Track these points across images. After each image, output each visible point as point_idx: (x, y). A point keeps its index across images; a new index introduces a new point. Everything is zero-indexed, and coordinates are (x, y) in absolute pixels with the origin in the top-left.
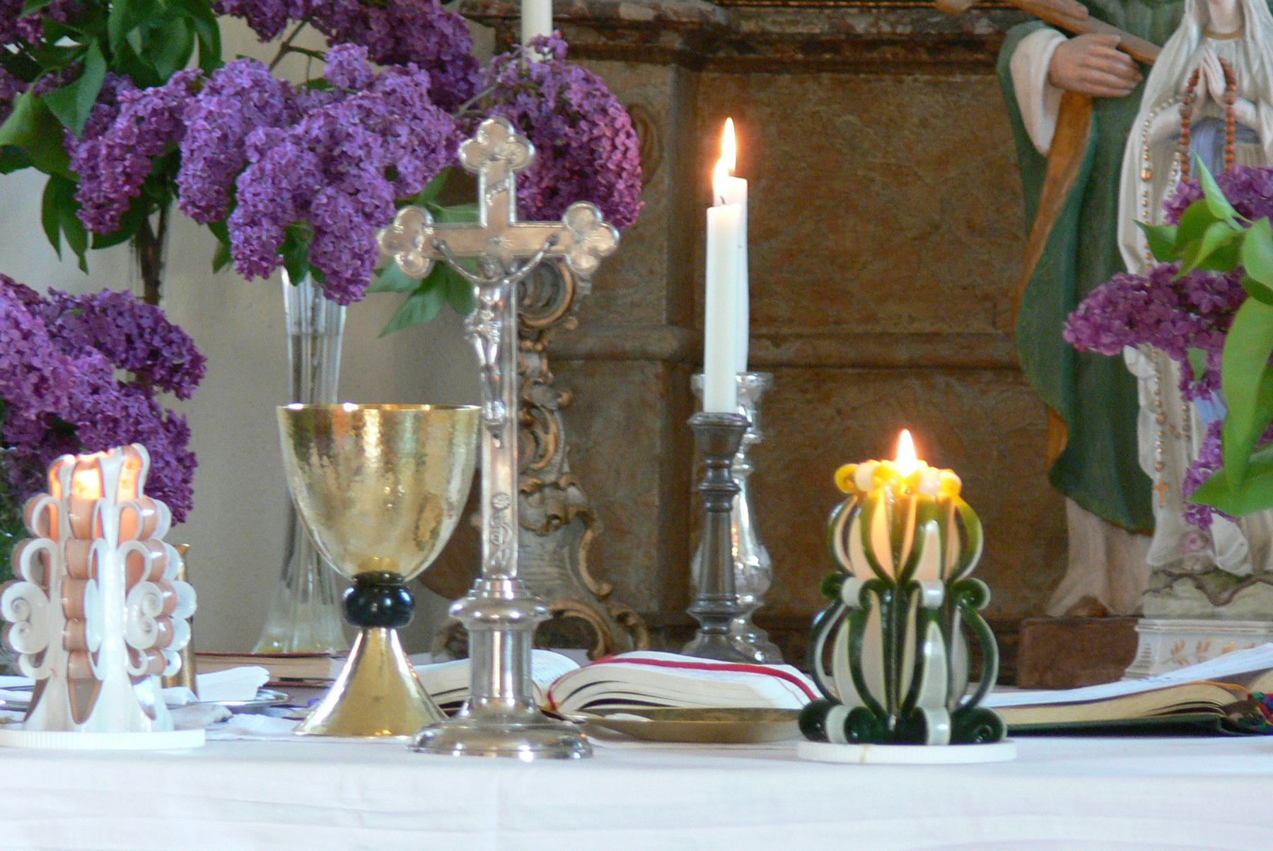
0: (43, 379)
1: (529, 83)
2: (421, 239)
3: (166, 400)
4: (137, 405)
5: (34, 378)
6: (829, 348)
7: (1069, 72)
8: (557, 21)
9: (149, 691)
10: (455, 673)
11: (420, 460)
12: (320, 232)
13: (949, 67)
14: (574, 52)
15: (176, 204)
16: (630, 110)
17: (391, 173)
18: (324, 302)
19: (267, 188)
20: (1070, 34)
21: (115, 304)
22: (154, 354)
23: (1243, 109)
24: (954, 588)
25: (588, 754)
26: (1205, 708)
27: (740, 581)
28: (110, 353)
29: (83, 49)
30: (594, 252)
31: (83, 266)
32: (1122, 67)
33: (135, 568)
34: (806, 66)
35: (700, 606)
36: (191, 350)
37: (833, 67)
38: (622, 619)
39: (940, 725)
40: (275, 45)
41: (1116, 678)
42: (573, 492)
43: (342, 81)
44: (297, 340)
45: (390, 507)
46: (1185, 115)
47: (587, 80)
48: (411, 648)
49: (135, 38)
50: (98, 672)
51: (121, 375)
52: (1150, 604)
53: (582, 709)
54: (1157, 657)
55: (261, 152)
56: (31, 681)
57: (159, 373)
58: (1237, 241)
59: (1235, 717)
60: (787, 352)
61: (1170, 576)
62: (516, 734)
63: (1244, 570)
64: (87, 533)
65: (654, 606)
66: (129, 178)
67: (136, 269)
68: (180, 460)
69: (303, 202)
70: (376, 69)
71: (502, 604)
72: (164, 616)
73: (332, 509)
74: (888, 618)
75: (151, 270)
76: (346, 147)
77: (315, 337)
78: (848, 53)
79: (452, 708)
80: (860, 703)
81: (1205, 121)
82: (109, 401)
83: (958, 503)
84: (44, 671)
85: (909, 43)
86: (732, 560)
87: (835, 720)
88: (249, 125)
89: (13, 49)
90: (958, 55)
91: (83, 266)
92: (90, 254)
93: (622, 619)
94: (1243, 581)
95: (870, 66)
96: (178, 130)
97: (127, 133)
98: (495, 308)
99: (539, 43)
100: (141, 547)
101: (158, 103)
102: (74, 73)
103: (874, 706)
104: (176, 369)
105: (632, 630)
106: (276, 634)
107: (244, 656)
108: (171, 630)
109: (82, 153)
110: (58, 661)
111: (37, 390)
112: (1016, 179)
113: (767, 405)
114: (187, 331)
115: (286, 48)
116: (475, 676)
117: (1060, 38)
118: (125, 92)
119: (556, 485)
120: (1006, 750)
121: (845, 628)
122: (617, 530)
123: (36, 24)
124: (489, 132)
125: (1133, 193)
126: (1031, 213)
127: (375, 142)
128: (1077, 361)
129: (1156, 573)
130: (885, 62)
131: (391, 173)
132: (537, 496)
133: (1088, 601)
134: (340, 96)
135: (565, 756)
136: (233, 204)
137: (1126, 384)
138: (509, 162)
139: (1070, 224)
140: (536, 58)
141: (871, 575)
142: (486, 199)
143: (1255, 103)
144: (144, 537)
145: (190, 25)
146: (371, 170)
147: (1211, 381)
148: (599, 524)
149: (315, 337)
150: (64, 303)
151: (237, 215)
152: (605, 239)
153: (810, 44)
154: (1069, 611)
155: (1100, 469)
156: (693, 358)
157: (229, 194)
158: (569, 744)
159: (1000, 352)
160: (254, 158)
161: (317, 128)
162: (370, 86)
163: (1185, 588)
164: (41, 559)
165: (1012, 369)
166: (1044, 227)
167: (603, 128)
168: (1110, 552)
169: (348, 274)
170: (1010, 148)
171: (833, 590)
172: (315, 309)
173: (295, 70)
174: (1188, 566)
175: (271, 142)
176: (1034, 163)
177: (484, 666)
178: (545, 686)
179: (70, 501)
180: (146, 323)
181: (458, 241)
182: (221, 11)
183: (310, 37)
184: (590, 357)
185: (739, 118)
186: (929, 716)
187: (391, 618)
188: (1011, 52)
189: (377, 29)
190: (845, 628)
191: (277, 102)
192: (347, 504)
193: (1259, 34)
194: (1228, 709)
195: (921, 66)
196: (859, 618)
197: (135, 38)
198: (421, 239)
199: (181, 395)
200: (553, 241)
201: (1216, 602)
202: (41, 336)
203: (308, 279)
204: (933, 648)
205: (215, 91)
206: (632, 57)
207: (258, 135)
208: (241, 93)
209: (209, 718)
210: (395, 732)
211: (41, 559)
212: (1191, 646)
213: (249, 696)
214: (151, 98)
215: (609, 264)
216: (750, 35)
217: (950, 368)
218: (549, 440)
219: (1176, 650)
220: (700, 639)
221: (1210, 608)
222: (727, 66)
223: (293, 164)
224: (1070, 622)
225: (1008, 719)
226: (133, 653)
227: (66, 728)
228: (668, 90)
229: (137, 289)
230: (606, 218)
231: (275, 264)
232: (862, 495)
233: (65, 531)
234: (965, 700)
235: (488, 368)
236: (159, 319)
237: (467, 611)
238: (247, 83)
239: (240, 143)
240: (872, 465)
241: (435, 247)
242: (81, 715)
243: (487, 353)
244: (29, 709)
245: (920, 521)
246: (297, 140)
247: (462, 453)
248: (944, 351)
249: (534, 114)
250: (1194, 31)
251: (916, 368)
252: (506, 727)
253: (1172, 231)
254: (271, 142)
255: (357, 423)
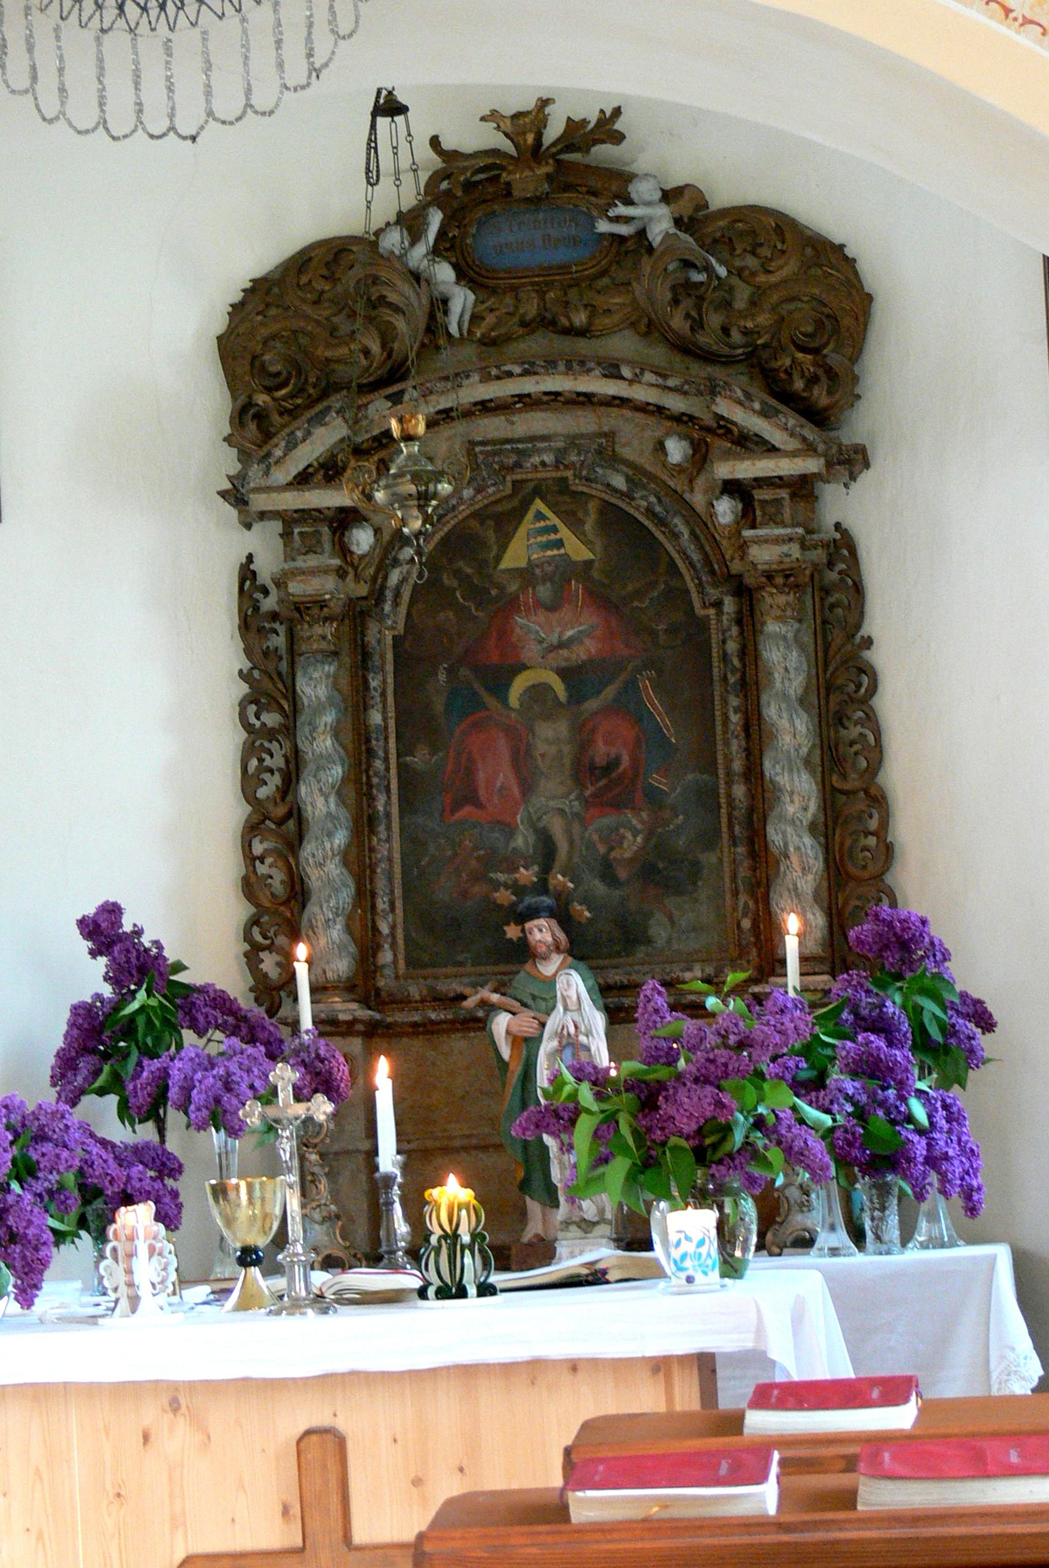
0: (113, 1178)
1: (306, 1048)
2: (257, 1113)
3: (169, 1182)
4: (157, 1185)
5: (109, 1178)
6: (430, 1144)
7: (515, 1029)
8: (314, 1023)
9: (163, 1299)
10: (279, 1283)
11: (263, 1199)
12: (225, 1111)
13: (469, 1030)
14: (322, 1034)
15: (170, 1103)
16: (345, 1056)
17: (252, 1087)
18: (229, 1140)
19: (203, 1096)
20: (514, 1014)
21: (147, 1146)
22: (164, 1164)
23: (583, 1039)
24: (474, 1236)
25: (336, 1311)
26: (578, 1276)
27: (399, 1237)
28: (146, 1165)
29: (128, 1047)
30: (325, 1113)
31: (134, 1131)
32: (535, 1026)
33: (152, 1250)
34: (414, 1033)
35: (384, 1248)
36: (178, 1162)
37: (423, 1033)
38: (355, 1256)
39: (472, 1290)
40: (205, 1040)
41: (549, 1264)
42: (333, 1207)
43: (231, 1052)
44: (220, 1156)
45: (253, 1219)
46: (560, 1042)
47: (327, 1045)
48: (265, 1274)
49: (149, 1041)
50: (139, 1293)
51: (152, 1173)
52: (560, 1235)
53: (334, 1294)
54: (564, 1255)
55: (200, 1082)
56: (114, 1299)
57: (166, 1172)
58: (576, 1090)
59: (590, 1278)
60: (413, 1146)
61: (567, 1224)
62: (306, 1306)
63: (596, 1219)
64: (131, 1239)
65: (368, 1250)
66: (149, 1095)
67: (156, 1131)
68: (176, 1205)
69: (218, 1101)
70: (244, 1046)
71: (297, 1254)
72: (165, 1269)
73: (229, 1221)
74: (449, 1249)
75: (161, 1131)
76: (234, 1078)
77: (227, 1153)
78: (429, 1027)
79: (281, 1297)
80: (440, 1284)
81: (568, 1044)
82: (147, 1185)
83: (474, 1202)
84: (119, 1294)
85: (453, 1022)
86: (395, 1230)
87: (431, 1292)
88: (195, 1071)
89: (102, 1048)
90: (472, 1025)
91: (134, 1131)
92: (137, 1127)
93: (355, 1256)
94: (595, 1224)
95: (438, 1032)
96: (168, 1075)
97: (147, 1078)
98: (287, 1138)
99: (307, 1032)
100: (154, 1242)
101: (159, 1065)
102: (125, 1055)
103: (446, 1284)
104: (173, 1169)
105: (359, 1260)
106: (219, 1271)
107: (205, 1281)
108: (168, 1274)
109: (131, 1087)
110: (123, 1290)
111: (111, 1183)
112: (497, 1072)
113: (405, 1168)
114: (176, 1154)
115: (209, 1040)
116: (289, 1284)
117: (510, 1016)
118: (146, 1062)
119: (325, 1205)
120: (501, 1298)
121: (433, 1254)
122: (352, 1220)
123: (110, 1038)
124: (281, 1069)
125: (542, 1073)
126: (504, 1085)
127: (245, 1075)
128: (526, 1145)
129: (561, 1223)
130: (443, 1030)
131: (252, 1087)
132: (318, 1210)
133: (537, 1236)
134: (230, 1058)
135: (326, 1313)
136: (190, 1103)
137: (545, 1149)
138: (289, 1080)
139: (519, 1088)
140: (306, 1037)
141: (441, 1233)
142: (281, 1095)
143: (587, 1036)
144: (155, 1238)
145: (171, 1035)
146: (244, 1086)
147: (571, 1147)
148: (344, 1219)
149: (227, 1153)
150: (126, 1146)
151: (192, 1107)
152: (329, 1108)
153: (415, 1025)
154: (530, 1241)
155: (537, 1182)
156: (374, 1152)
157: (188, 1099)
158: (328, 1308)
159: (495, 1140)
160: (197, 1084)
161: (222, 1071)
162: (242, 1053)
163: (573, 1228)
164: (114, 1250)
165: (499, 1147)
166: (510, 1090)
167: (334, 1063)
168: (544, 1215)
169: (237, 1127)
170: (494, 1062)
171: (428, 1241)
172: (226, 1142)
173: (213, 1049)
174: (574, 1219)
175: (204, 1077)
176: (504, 1065)
177: (291, 1280)
178: (318, 1286)
179: (124, 1227)
180: (160, 1152)
181: (271, 1112)
182: (182, 1027)
183: (218, 1035)
184: (336, 1154)
185: (388, 1055)
186: (468, 1287)
187: (257, 1262)
188: (491, 1022)
189: (244, 1031)
190: (433, 1254)
191: (206, 1062)
192: (235, 1219)
193: (587, 1009)
194: (587, 1275)
195: (458, 1030)
196: (438, 1250)
197: (149, 1041)
198: (257, 1113)
199: (175, 1180)
200: (308, 1109)
201: (586, 1233)
202: (111, 1161)
203: (223, 1130)
204: (468, 1259)
205: (181, 1059)
206: (343, 1035)
207: (199, 1076)
208: (191, 1059)
209: (186, 1308)
210: (260, 1308)
211: (114, 1250)
212: (577, 1251)
213: (204, 1298)
214: (156, 1064)
215: (335, 1116)
216: (391, 1024)
217: (476, 1148)
218: (322, 1187)
219: (572, 1252)
220: (385, 1261)
221: (583, 1235)
222: (383, 1036)
223: (212, 1086)
224: (530, 1245)
225: (499, 1286)
226: (153, 1285)
227: (128, 1316)
228: (360, 1047)
229: (156, 1138)
230: (329, 1099)
231: (209, 1125)
232: (436, 1202)
233: (123, 1238)
234: (482, 1279)
235: (286, 1162)
236: (164, 1150)
237: (284, 1258)
238: (193, 1055)
239: (192, 1079)
240: (439, 1189)
241: (263, 1117)
242: (134, 1311)
243: (285, 1156)
244: (113, 1310)
245: (459, 1210)
246: (214, 1077)
247: (279, 1195)
248: (474, 1141)
249: (307, 1060)
250: (561, 1009)
251: (465, 1149)
252: (302, 1303)
253: (551, 1089)
254: (204, 1077)
255: (237, 1187)
